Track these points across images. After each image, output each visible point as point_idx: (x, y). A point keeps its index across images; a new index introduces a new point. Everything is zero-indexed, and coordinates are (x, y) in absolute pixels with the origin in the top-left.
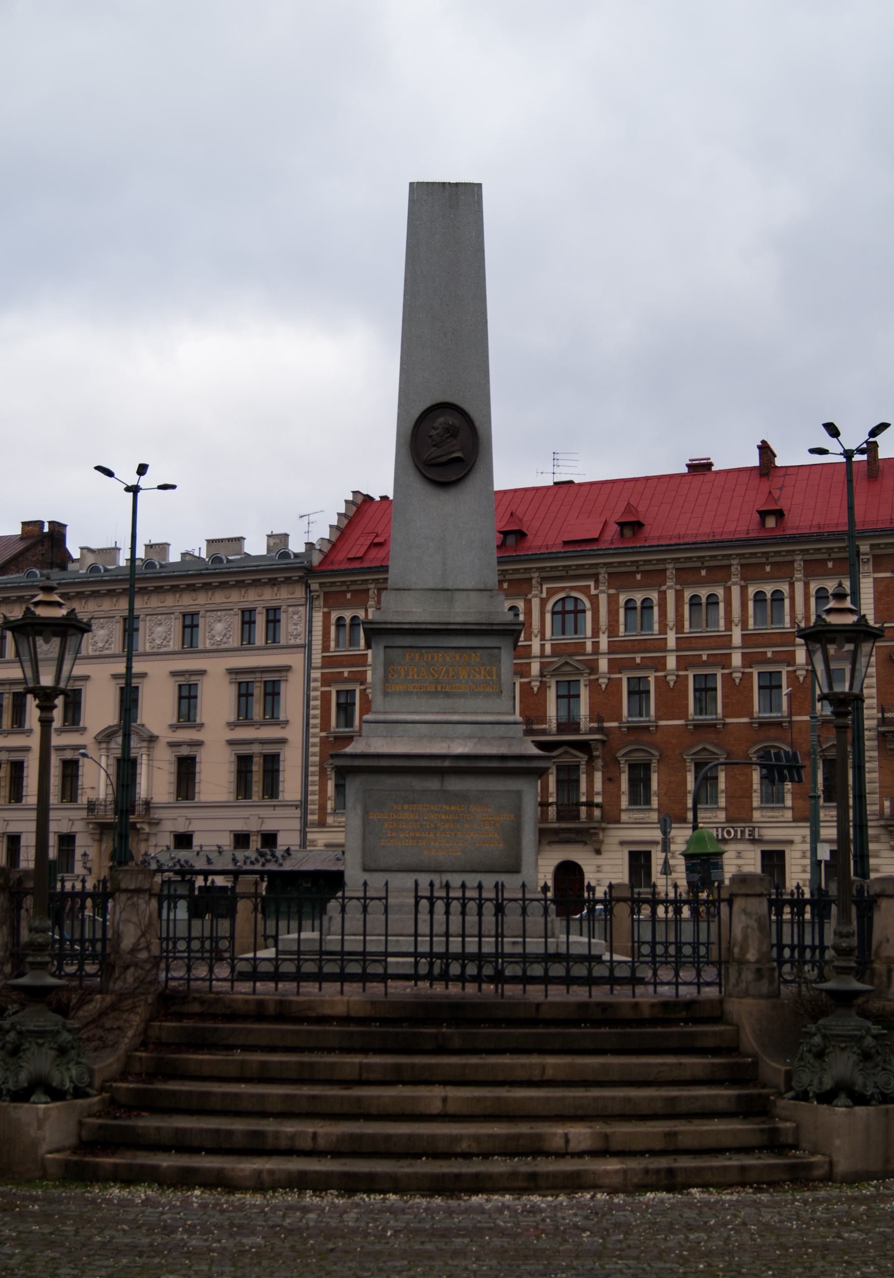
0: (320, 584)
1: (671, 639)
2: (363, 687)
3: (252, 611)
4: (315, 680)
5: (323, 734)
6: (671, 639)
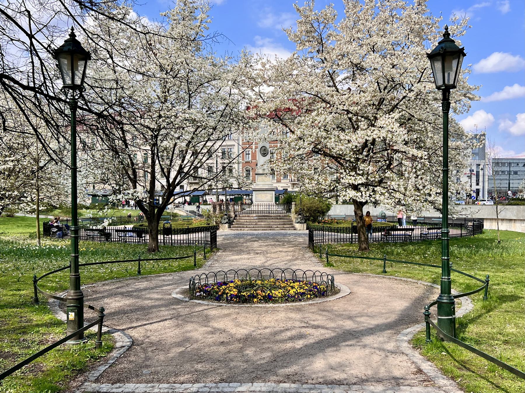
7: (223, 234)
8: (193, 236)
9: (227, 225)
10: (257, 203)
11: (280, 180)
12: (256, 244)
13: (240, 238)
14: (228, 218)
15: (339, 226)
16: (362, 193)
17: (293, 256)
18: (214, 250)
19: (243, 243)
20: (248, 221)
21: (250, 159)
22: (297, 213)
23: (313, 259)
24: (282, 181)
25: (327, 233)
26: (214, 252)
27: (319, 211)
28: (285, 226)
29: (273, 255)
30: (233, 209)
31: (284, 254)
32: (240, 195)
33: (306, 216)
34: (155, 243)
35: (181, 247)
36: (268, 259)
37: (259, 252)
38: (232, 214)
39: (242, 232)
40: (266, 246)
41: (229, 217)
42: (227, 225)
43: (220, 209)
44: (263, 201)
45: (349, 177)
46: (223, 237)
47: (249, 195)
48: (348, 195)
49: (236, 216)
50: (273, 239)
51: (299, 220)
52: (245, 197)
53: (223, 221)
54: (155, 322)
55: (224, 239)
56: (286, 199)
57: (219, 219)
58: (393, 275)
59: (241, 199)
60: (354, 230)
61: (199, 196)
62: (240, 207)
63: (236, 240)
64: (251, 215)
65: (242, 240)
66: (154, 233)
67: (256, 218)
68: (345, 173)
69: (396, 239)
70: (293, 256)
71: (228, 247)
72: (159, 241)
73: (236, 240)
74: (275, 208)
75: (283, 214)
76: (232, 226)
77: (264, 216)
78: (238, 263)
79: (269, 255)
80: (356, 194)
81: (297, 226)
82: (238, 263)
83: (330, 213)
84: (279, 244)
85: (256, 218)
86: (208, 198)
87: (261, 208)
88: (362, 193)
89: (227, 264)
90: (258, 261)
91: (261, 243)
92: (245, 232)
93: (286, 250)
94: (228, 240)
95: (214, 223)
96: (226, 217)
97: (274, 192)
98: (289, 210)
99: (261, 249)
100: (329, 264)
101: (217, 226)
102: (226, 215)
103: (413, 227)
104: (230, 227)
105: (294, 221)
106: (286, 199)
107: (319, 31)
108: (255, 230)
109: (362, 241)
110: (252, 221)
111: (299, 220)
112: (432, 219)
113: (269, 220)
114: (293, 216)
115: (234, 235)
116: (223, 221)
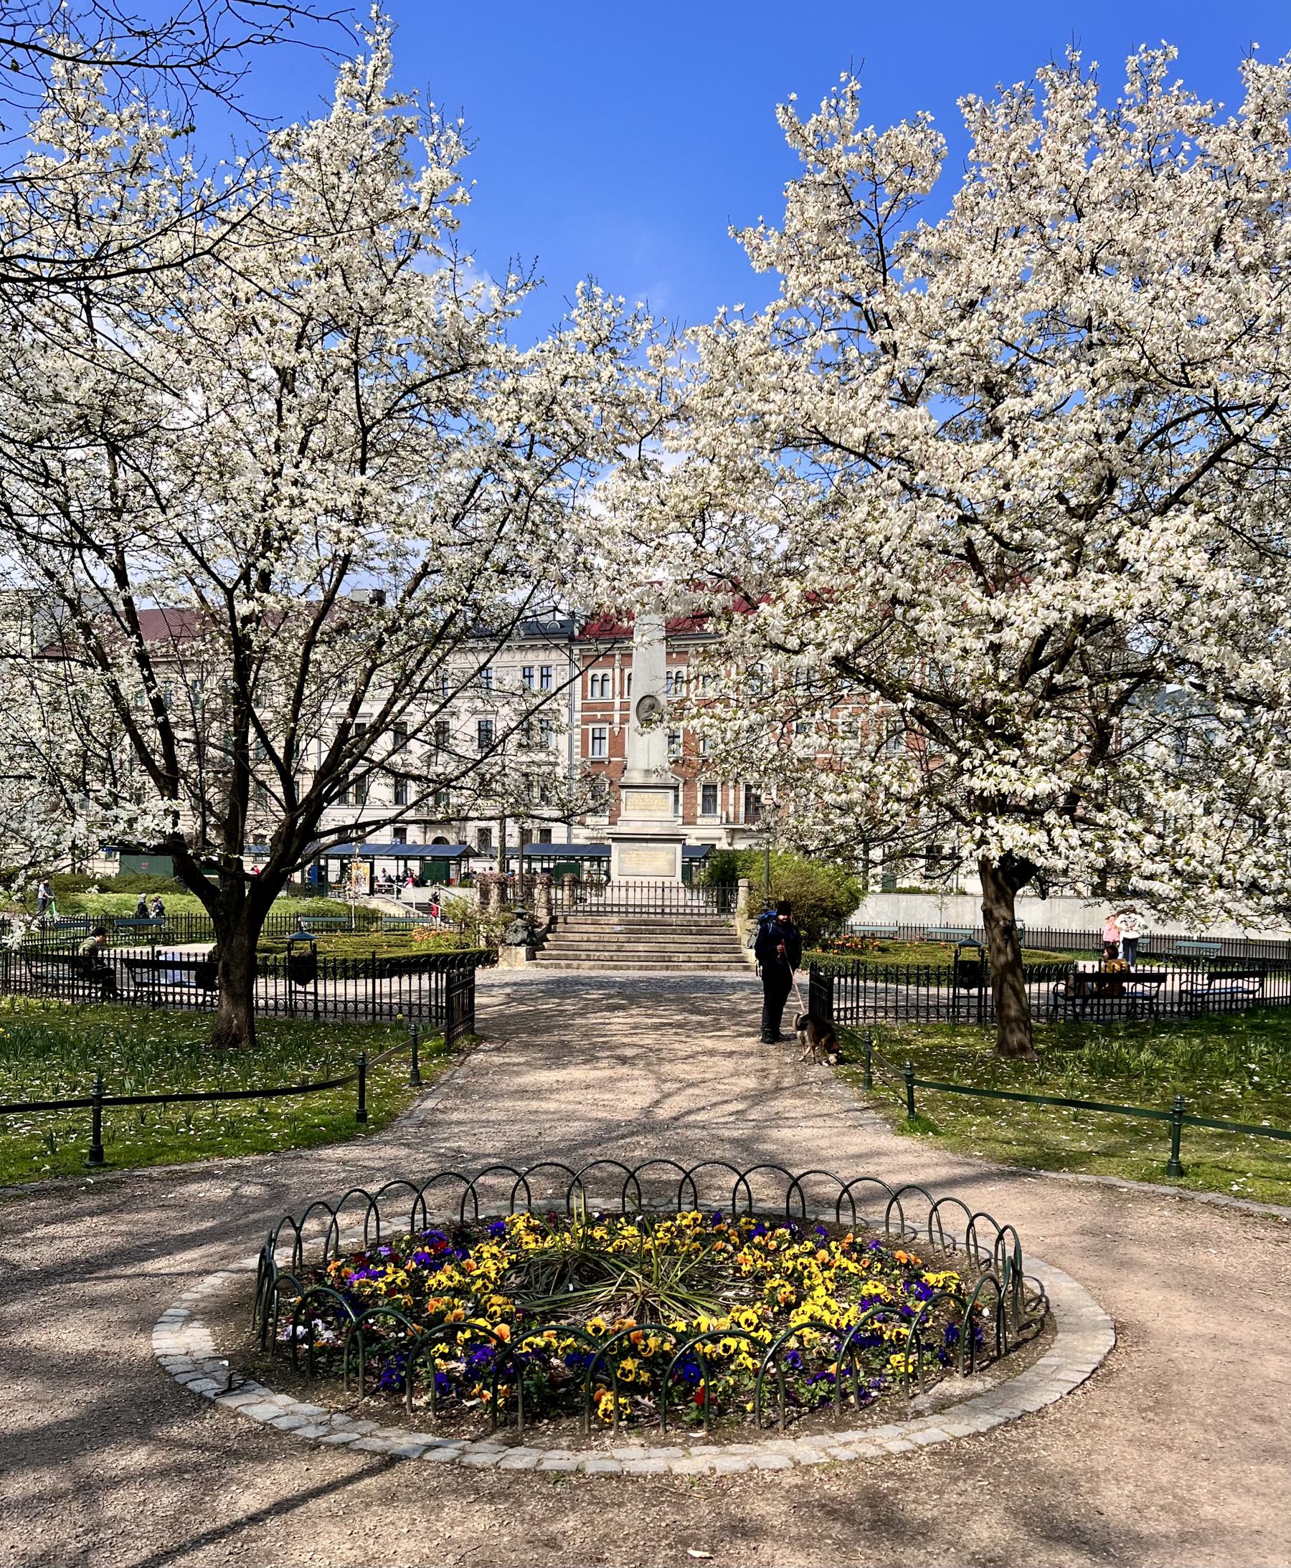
1: (617, 701)
6: (617, 701)
7: (508, 979)
8: (389, 986)
9: (522, 951)
10: (623, 880)
11: (695, 816)
12: (618, 1021)
13: (563, 996)
14: (526, 928)
15: (890, 959)
16: (1049, 832)
17: (764, 1073)
18: (463, 1042)
19: (573, 1016)
20: (592, 937)
23: (838, 1089)
24: (699, 821)
25: (870, 984)
26: (460, 1051)
28: (715, 957)
29: (680, 1070)
31: (729, 1065)
32: (572, 858)
34: (242, 1012)
35: (344, 1028)
36: (668, 1087)
37: (629, 1052)
38: (542, 916)
39: (572, 973)
40: (657, 1027)
41: (532, 923)
42: (522, 951)
44: (645, 874)
45: (999, 770)
46: (508, 990)
47: (599, 860)
48: (993, 840)
49: (554, 920)
52: (587, 864)
53: (512, 938)
55: (510, 999)
57: (498, 931)
58: (1217, 1189)
59: (577, 869)
60: (966, 973)
61: (448, 858)
63: (550, 1004)
64: (603, 919)
65: (570, 1006)
66: (237, 973)
67: (618, 928)
68: (980, 753)
69: (1108, 1010)
70: (764, 1073)
71: (516, 1032)
72: (262, 1003)
73: (550, 1004)
74: (681, 897)
75: (709, 918)
76: (538, 954)
77: (645, 923)
78: (545, 1105)
79: (667, 1068)
80: (1026, 837)
82: (545, 1105)
83: (854, 919)
84: (699, 1023)
85: (618, 928)
86: (477, 866)
87: (636, 897)
88: (1049, 832)
89: (498, 1110)
90: (631, 1095)
91: (636, 1016)
92: (584, 973)
93: (730, 1046)
94: (521, 1001)
95: (483, 943)
96: (519, 922)
97: (679, 847)
98: (725, 906)
99: (635, 1039)
100: (916, 1123)
101: (489, 953)
102: (520, 916)
103: (1162, 970)
104: (531, 957)
105: (744, 941)
106: (718, 874)
107: (872, 218)
108: (615, 968)
109: (1009, 1020)
110: (606, 937)
112: (1179, 943)
113: (660, 938)
115: (547, 983)
116: (512, 938)
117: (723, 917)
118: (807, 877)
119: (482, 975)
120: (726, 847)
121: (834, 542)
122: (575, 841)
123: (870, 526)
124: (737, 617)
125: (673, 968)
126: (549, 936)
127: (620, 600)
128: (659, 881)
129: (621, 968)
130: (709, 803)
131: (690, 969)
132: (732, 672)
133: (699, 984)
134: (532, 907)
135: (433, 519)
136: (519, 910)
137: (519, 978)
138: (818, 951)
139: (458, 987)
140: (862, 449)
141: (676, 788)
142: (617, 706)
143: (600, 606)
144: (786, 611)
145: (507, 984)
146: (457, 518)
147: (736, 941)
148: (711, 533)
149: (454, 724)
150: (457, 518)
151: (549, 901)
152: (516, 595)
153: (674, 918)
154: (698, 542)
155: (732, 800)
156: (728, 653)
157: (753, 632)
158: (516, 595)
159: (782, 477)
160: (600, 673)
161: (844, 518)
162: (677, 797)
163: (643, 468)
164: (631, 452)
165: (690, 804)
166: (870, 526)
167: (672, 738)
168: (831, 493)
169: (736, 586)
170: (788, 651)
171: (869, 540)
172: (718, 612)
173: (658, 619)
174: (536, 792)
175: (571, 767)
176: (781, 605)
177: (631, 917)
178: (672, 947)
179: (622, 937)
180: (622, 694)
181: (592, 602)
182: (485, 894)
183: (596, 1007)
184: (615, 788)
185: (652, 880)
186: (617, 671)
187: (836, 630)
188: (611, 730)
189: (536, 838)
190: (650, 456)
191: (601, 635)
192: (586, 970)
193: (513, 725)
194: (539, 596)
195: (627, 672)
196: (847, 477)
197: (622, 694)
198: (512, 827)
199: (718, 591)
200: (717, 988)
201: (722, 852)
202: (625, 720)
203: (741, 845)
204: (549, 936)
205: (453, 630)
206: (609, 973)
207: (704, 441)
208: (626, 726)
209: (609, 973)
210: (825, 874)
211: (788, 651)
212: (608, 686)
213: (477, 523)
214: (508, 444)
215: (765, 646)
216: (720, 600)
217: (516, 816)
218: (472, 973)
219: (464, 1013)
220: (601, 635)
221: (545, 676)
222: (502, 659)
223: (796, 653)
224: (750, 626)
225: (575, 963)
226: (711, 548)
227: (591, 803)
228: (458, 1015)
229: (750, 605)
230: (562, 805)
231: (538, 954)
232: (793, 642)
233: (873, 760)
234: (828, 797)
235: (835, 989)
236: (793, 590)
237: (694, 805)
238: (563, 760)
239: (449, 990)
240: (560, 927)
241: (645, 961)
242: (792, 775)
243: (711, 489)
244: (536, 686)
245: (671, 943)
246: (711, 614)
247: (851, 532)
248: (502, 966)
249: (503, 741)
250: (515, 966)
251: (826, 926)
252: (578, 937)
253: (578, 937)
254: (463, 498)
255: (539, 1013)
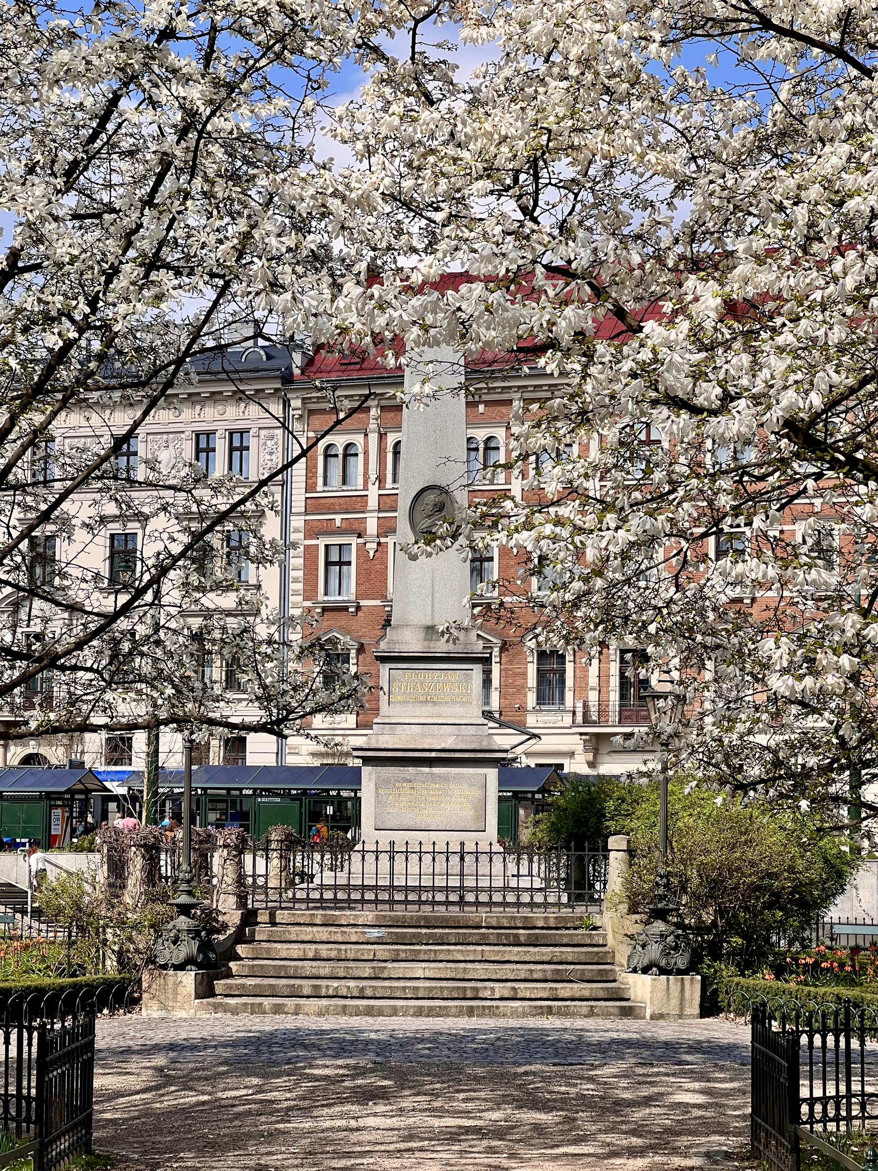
0: (303, 399)
1: (373, 493)
2: (361, 541)
3: (209, 434)
4: (296, 531)
5: (308, 604)
6: (373, 493)
7: (160, 1036)
11: (522, 709)
14: (195, 933)
19: (287, 1114)
20: (324, 951)
21: (350, 592)
22: (649, 903)
27: (777, 895)
28: (565, 989)
30: (230, 877)
33: (701, 929)
38: (228, 909)
39: (287, 1023)
41: (207, 924)
42: (188, 979)
43: (152, 865)
44: (430, 826)
46: (160, 1060)
49: (249, 918)
50: (493, 1079)
51: (654, 951)
53: (168, 953)
54: (138, 1092)
55: (164, 1079)
56: (571, 823)
57: (142, 941)
62: (276, 862)
63: (239, 1090)
64: (346, 916)
65: (281, 1091)
67: (375, 933)
76: (220, 985)
77: (426, 920)
81: (642, 988)
83: (836, 912)
84: (538, 1129)
85: (375, 933)
87: (408, 872)
94: (187, 1083)
95: (111, 963)
96: (183, 922)
97: (492, 774)
98: (582, 886)
102: (185, 910)
104: (205, 991)
105: (621, 958)
106: (571, 823)
108: (369, 1012)
110: (351, 951)
111: (654, 951)
114: (613, 922)
115: (234, 1044)
116: (168, 953)
117: (580, 910)
118: (742, 833)
119: (108, 1029)
120: (584, 770)
121: (781, 208)
122: (291, 760)
123: (851, 180)
124: (601, 348)
125: (483, 1012)
126: (241, 949)
127: (381, 321)
128: (455, 838)
129: (380, 1013)
130: (550, 686)
131: (515, 1014)
132: (594, 446)
133: (534, 1045)
134: (208, 892)
135: (31, 170)
136: (184, 899)
137: (182, 1034)
138: (765, 979)
139: (59, 1061)
140: (836, 36)
141: (486, 661)
142: (373, 502)
143: (344, 331)
144: (695, 334)
145: (156, 1048)
146: (73, 170)
147: (604, 959)
148: (549, 195)
149: (63, 551)
150: (73, 170)
151: (240, 879)
152: (186, 304)
153: (483, 913)
154: (524, 209)
155: (595, 678)
156: (583, 412)
157: (634, 375)
158: (186, 304)
159: (683, 89)
160: (339, 441)
161: (803, 166)
162: (487, 673)
163: (420, 81)
164: (397, 46)
165: (513, 687)
166: (851, 180)
167: (479, 562)
168: (774, 116)
169: (599, 292)
170: (695, 410)
171: (851, 205)
172: (566, 340)
173: (450, 353)
174: (216, 672)
175: (284, 621)
176: (684, 326)
177: (399, 911)
178: (480, 970)
179: (382, 951)
180: (381, 479)
181: (329, 326)
182: (117, 868)
183: (327, 1093)
184: (368, 657)
185: (441, 838)
186: (373, 438)
187: (791, 370)
188: (362, 548)
189: (216, 755)
190: (434, 55)
191: (347, 379)
192: (310, 1017)
193: (176, 549)
194: (227, 309)
195: (391, 439)
196: (806, 85)
197: (381, 479)
198: (172, 743)
199: (566, 303)
200: (571, 1052)
201: (579, 779)
202: (387, 528)
203: (614, 767)
204: (241, 949)
205: (65, 375)
206: (356, 1022)
207: (538, 26)
208: (390, 540)
209: (356, 1022)
210: (775, 835)
211: (695, 410)
212: (357, 465)
213: (114, 179)
214: (168, 34)
215: (655, 403)
216: (570, 319)
217: (180, 722)
218: (90, 1029)
219: (73, 1110)
220: (347, 379)
221: (238, 447)
222: (161, 416)
223: (714, 413)
224: (627, 366)
225: (290, 1003)
226: (547, 221)
227: (322, 697)
228: (59, 1118)
229: (625, 325)
230: (266, 698)
231: (220, 985)
232: (709, 393)
233: (865, 613)
234: (778, 683)
235: (804, 1054)
236: (706, 298)
237: (522, 689)
238: (271, 606)
239: (43, 1065)
240: (262, 932)
241: (429, 999)
242: (714, 636)
243: (550, 122)
244: (219, 469)
245: (475, 962)
246: (552, 344)
247: (814, 192)
248: (150, 1010)
249: (156, 581)
250: (174, 1009)
251: (781, 926)
252: (295, 950)
253: (295, 950)
254: (85, 133)
255: (218, 1106)
